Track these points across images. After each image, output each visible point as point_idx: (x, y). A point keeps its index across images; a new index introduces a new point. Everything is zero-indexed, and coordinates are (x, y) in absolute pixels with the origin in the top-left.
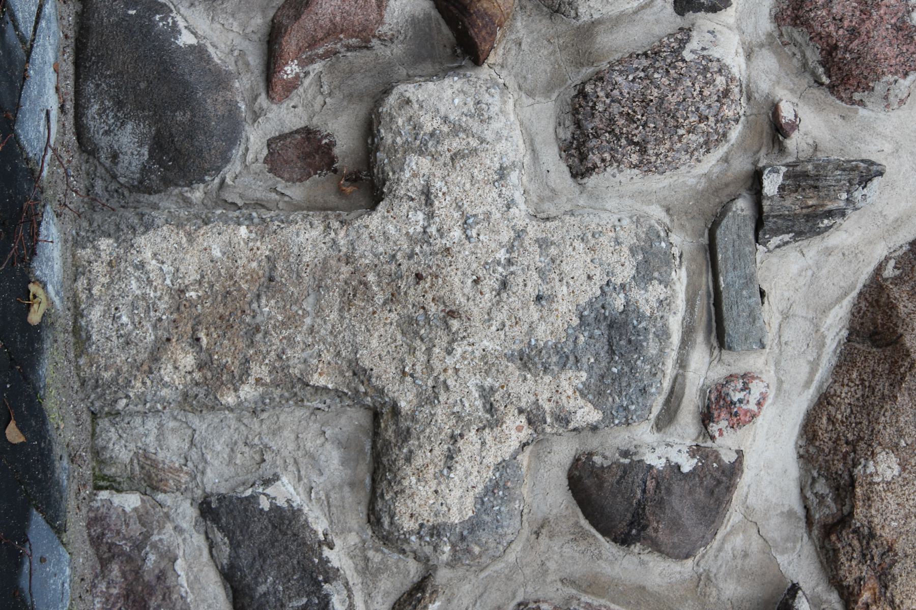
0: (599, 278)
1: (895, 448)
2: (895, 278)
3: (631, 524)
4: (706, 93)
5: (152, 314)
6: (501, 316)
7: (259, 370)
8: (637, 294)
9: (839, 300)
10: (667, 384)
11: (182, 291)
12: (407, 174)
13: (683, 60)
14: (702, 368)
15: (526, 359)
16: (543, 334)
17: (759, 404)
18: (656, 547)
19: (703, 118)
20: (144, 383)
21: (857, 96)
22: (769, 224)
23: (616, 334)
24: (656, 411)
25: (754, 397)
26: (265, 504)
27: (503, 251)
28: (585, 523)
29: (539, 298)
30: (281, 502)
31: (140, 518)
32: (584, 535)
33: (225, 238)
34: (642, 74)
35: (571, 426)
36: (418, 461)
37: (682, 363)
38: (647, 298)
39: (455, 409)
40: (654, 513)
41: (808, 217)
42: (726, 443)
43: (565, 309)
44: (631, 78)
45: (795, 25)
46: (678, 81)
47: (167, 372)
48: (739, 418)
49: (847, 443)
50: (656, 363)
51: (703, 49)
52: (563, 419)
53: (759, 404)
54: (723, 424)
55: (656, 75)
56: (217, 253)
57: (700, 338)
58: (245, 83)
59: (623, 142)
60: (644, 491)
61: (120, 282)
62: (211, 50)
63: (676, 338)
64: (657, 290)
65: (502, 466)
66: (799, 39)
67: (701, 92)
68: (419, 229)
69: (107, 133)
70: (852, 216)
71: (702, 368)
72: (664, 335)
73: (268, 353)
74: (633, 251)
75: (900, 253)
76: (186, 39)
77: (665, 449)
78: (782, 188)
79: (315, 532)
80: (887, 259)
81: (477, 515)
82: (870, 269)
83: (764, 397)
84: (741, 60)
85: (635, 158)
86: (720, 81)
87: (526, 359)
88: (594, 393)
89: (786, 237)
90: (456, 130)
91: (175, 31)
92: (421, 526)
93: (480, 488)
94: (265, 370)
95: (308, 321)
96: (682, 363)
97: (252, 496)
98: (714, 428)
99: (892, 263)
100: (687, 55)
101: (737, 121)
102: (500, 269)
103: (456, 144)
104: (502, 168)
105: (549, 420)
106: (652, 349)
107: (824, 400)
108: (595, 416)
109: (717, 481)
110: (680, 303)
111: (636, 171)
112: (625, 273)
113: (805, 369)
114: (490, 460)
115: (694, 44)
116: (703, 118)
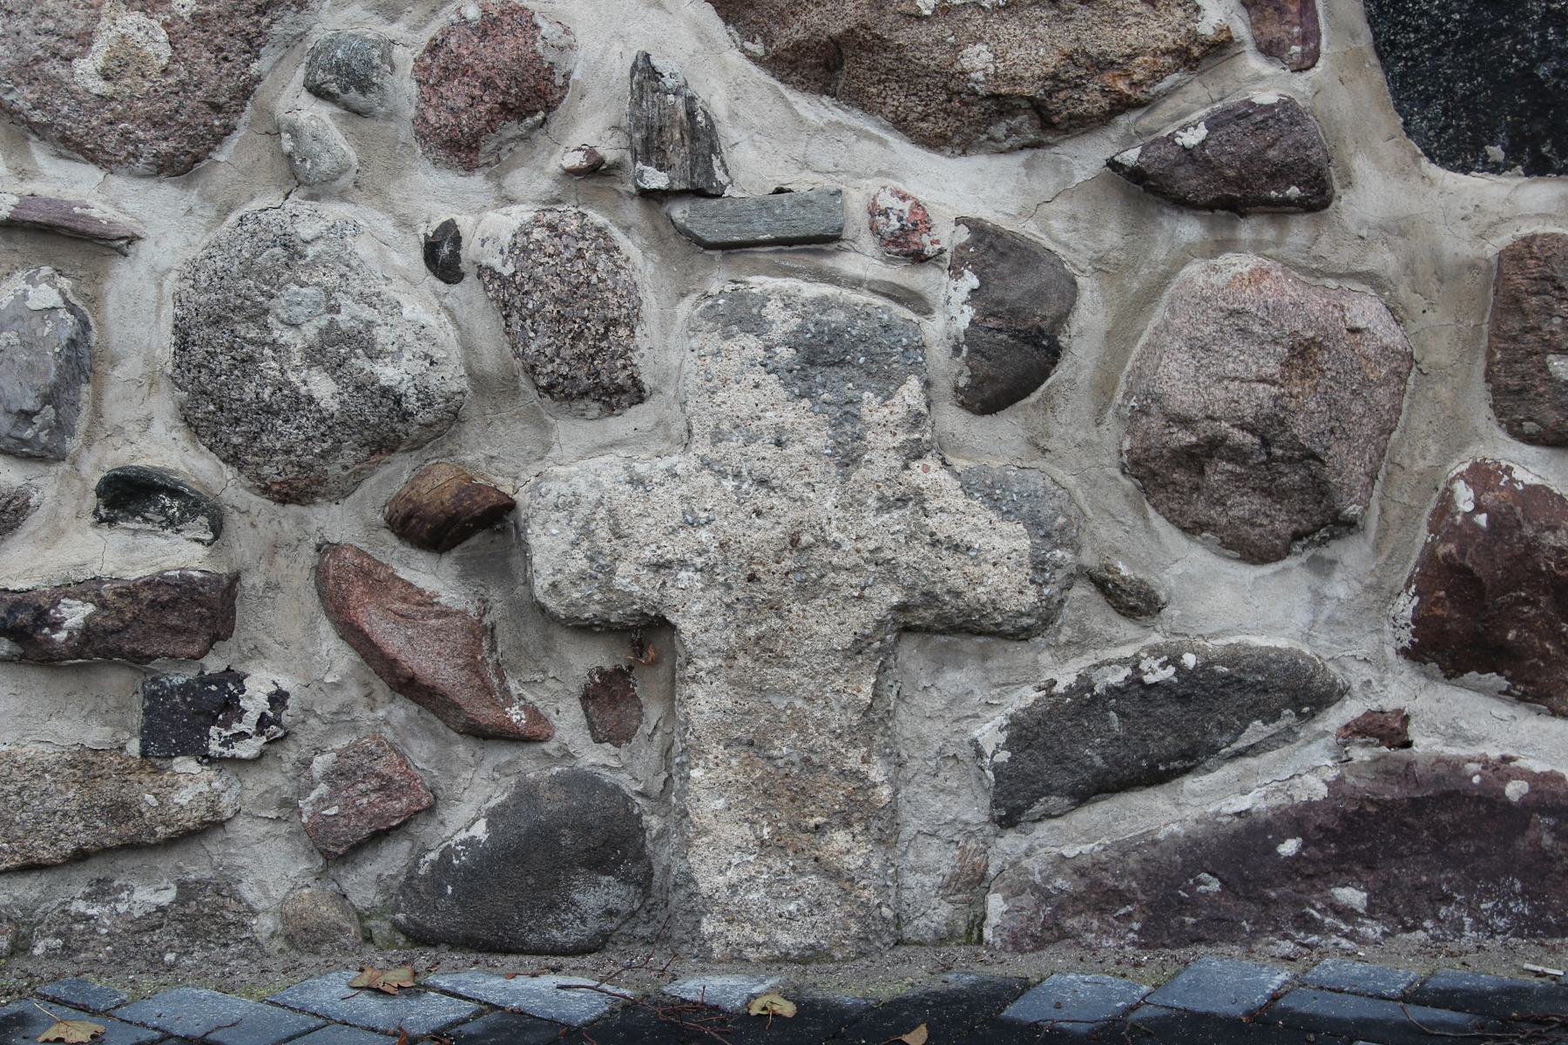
0: (758, 375)
2: (765, 42)
3: (1037, 346)
4: (551, 250)
6: (798, 488)
7: (853, 760)
9: (788, 105)
10: (880, 301)
12: (636, 588)
13: (514, 275)
14: (863, 261)
16: (820, 440)
17: (904, 198)
18: (1062, 318)
20: (865, 887)
21: (559, 81)
22: (701, 182)
23: (821, 357)
24: (908, 314)
26: (1004, 756)
27: (724, 483)
28: (1034, 397)
31: (1015, 895)
32: (1047, 398)
33: (703, 794)
34: (529, 322)
36: (960, 583)
38: (781, 322)
42: (946, 236)
43: (793, 415)
46: (537, 282)
47: (853, 862)
48: (920, 221)
49: (950, 101)
50: (855, 313)
51: (502, 252)
53: (904, 198)
54: (925, 239)
56: (720, 804)
57: (827, 263)
58: (531, 766)
59: (604, 344)
62: (492, 803)
63: (828, 290)
64: (773, 310)
67: (550, 256)
68: (698, 576)
69: (583, 922)
71: (863, 261)
72: (823, 304)
73: (833, 749)
74: (728, 336)
75: (736, 36)
76: (480, 831)
77: (953, 304)
78: (660, 168)
81: (1022, 519)
84: (515, 209)
85: (623, 332)
86: (538, 234)
87: (848, 459)
88: (887, 384)
89: (716, 163)
90: (586, 532)
91: (470, 843)
93: (992, 515)
94: (853, 753)
95: (799, 703)
96: (856, 283)
97: (994, 771)
98: (930, 250)
99: (748, 45)
100: (507, 271)
102: (745, 486)
103: (603, 533)
105: (917, 436)
106: (838, 317)
107: (901, 125)
108: (914, 383)
109: (990, 247)
111: (637, 330)
112: (752, 346)
113: (866, 145)
114: (960, 502)
115: (496, 262)
116: (580, 254)
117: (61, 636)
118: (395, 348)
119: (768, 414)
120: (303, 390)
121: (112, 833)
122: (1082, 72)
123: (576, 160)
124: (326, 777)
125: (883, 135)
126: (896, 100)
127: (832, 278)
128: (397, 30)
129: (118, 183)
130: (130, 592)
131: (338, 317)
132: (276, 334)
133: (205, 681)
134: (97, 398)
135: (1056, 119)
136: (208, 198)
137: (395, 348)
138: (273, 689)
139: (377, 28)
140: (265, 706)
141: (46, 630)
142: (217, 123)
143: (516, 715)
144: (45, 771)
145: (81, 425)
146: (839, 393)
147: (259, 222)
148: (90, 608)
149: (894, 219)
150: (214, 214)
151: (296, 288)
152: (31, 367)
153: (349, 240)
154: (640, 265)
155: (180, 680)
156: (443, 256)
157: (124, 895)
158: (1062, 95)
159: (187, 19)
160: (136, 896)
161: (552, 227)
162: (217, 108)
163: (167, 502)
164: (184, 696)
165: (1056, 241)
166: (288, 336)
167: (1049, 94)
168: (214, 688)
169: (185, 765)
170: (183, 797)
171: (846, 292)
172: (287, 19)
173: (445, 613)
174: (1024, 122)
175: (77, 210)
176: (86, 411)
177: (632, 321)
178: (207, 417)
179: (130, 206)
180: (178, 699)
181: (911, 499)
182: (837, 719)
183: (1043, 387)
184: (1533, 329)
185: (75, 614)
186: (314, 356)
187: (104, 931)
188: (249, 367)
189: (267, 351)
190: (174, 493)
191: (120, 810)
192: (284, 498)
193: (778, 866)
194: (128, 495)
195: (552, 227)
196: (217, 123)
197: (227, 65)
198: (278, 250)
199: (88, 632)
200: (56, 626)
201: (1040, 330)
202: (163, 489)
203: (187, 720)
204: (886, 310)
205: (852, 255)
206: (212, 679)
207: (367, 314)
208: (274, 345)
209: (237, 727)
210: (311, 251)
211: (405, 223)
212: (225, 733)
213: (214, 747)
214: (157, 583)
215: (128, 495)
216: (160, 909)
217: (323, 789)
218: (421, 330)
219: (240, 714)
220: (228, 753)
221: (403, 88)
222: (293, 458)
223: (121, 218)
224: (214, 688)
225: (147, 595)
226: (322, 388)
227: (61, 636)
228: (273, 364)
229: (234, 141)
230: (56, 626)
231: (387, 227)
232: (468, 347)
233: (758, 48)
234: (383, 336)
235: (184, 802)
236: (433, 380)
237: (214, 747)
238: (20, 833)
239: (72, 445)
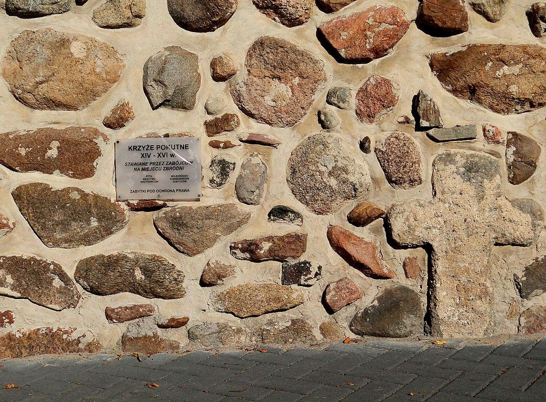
0: (455, 175)
1: (508, 86)
2: (452, 86)
3: (531, 166)
4: (396, 144)
5: (464, 313)
6: (467, 206)
7: (482, 281)
8: (459, 164)
9: (458, 103)
10: (487, 155)
11: (457, 304)
12: (421, 235)
13: (386, 151)
14: (480, 143)
15: (481, 198)
16: (472, 193)
17: (493, 127)
18: (537, 158)
19: (405, 144)
20: (486, 316)
21: (396, 98)
22: (437, 125)
23: (471, 169)
24: (495, 158)
25: (491, 128)
26: (524, 279)
27: (446, 205)
28: (529, 179)
29: (461, 194)
30: (523, 274)
31: (528, 317)
32: (533, 180)
33: (440, 291)
34: (390, 163)
35: (437, 162)
36: (512, 231)
37: (480, 150)
38: (460, 161)
39: (496, 219)
40: (529, 158)
41: (435, 113)
42: (504, 137)
43: (466, 186)
44: (391, 166)
45: (374, 117)
46: (392, 152)
47: (482, 309)
48: (498, 133)
49: (506, 100)
50: (481, 158)
51: (382, 145)
52: (499, 187)
53: (493, 127)
54: (500, 138)
55: (391, 159)
56: (445, 293)
57: (472, 145)
58: (385, 284)
59: (412, 169)
60: (522, 162)
61: (462, 324)
62: (378, 295)
63: (473, 152)
64: (458, 158)
65: (513, 206)
66: (379, 116)
67: (396, 145)
68: (438, 231)
69: (406, 327)
70: (434, 100)
71: (480, 143)
72: (472, 156)
73: (477, 277)
74: (445, 165)
75: (443, 85)
76: (376, 303)
77: (507, 154)
78: (427, 121)
79: (533, 263)
80: (445, 88)
81: (528, 213)
82: (449, 93)
83: (490, 125)
84: (385, 133)
85: (417, 165)
86: (392, 139)
87: (481, 198)
88: (491, 177)
89: (440, 119)
90: (407, 219)
91: (373, 307)
92: (532, 230)
93: (520, 212)
94: (482, 278)
95: (467, 265)
96: (480, 150)
97: (522, 283)
98: (501, 141)
99: (447, 87)
100: (384, 150)
101: (404, 134)
102: (451, 206)
103: (412, 219)
104: (419, 206)
105: (499, 191)
106: (477, 159)
107: (491, 108)
108: (498, 176)
109: (516, 138)
110: (461, 151)
111: (420, 164)
112: (453, 168)
113: (480, 113)
114: (512, 208)
115: (381, 147)
116: (405, 144)
117: (262, 252)
118: (353, 171)
119: (457, 186)
120: (328, 184)
121: (275, 306)
122: (542, 91)
123: (402, 119)
124: (334, 289)
125: (485, 109)
126: (489, 100)
127: (471, 148)
128: (351, 86)
129: (275, 129)
130: (281, 239)
131: (338, 164)
132: (320, 168)
133: (300, 263)
134: (268, 187)
135: (534, 104)
136: (298, 132)
137: (353, 171)
138: (318, 266)
139: (345, 85)
140: (317, 270)
141: (258, 250)
142: (302, 112)
143: (385, 271)
144: (256, 289)
145: (264, 195)
146: (477, 180)
147: (315, 139)
148: (271, 244)
149: (491, 132)
150: (300, 137)
151: (326, 156)
152: (253, 179)
153: (340, 142)
154: (420, 147)
155: (293, 263)
156: (364, 146)
157: (277, 323)
158: (537, 97)
159: (296, 85)
160: (280, 324)
161: (396, 138)
162: (303, 108)
163: (290, 214)
164: (294, 268)
165: (535, 138)
166: (323, 169)
167: (533, 97)
168: (303, 265)
169: (294, 286)
170: (294, 296)
171: (477, 153)
172: (322, 84)
173: (366, 243)
174: (527, 106)
175: (265, 137)
176: (265, 190)
177: (419, 162)
178: (300, 193)
179: (279, 136)
180: (292, 269)
181: (498, 208)
182: (478, 269)
183: (531, 177)
184: (74, 211)
185: (266, 246)
186: (330, 174)
187: (272, 333)
188: (312, 178)
189: (318, 173)
190: (293, 212)
191: (278, 299)
192: (319, 213)
193: (461, 310)
194: (279, 212)
195: (396, 138)
196: (302, 112)
197: (307, 97)
198: (321, 146)
199: (270, 250)
200: (261, 249)
201: (532, 161)
202: (289, 211)
203: (296, 274)
204: (489, 157)
205: (479, 142)
206: (302, 263)
207: (345, 162)
208: (319, 171)
209: (309, 276)
210: (330, 146)
211: (353, 137)
212: (305, 278)
213: (302, 282)
214: (289, 236)
215: (279, 212)
216: (287, 327)
217: (333, 293)
218: (360, 167)
219: (309, 272)
220: (306, 283)
221: (353, 102)
222: (323, 202)
223: (276, 138)
224: (303, 265)
225: (286, 240)
226: (333, 182)
227: (262, 252)
228: (319, 177)
229: (306, 117)
230: (261, 249)
231: (349, 139)
232: (371, 171)
233: (450, 88)
234: (350, 169)
235: (295, 297)
236: (362, 179)
237: (302, 282)
238: (250, 307)
239: (262, 200)
